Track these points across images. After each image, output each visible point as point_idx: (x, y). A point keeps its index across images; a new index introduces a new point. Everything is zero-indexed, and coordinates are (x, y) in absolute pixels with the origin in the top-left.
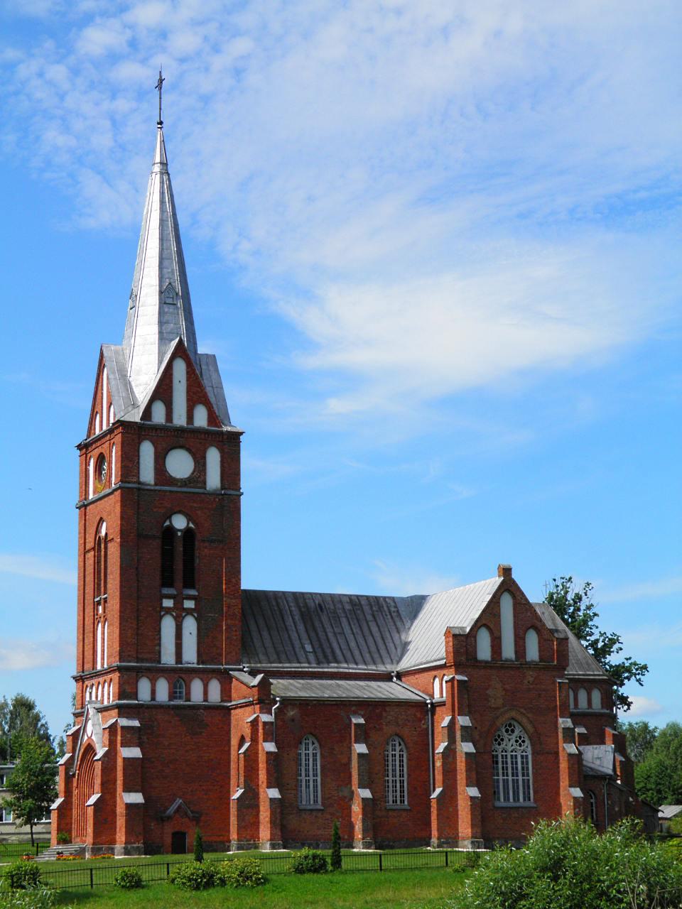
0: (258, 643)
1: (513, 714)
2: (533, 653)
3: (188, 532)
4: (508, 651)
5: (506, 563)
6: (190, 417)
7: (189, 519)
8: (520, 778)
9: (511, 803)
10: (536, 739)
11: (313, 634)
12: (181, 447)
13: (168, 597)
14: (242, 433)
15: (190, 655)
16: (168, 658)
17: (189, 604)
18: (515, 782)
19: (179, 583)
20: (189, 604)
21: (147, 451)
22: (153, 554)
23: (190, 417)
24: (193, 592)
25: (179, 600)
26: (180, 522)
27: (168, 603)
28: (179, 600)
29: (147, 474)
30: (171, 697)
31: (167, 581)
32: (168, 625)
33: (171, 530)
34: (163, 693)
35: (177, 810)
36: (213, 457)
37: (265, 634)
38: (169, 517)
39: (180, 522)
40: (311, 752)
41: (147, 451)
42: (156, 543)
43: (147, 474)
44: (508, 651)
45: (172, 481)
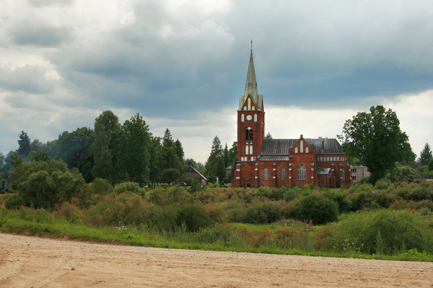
0: (266, 150)
1: (302, 163)
2: (307, 151)
3: (251, 130)
4: (302, 151)
5: (302, 134)
6: (251, 109)
7: (251, 128)
8: (304, 175)
9: (302, 179)
10: (307, 168)
11: (278, 148)
12: (249, 114)
13: (247, 142)
15: (251, 153)
16: (247, 153)
17: (251, 143)
18: (301, 176)
19: (249, 140)
20: (251, 143)
21: (243, 116)
22: (244, 135)
23: (251, 109)
24: (252, 141)
25: (249, 143)
26: (249, 128)
27: (247, 143)
28: (249, 143)
29: (243, 120)
30: (247, 160)
31: (247, 139)
32: (247, 147)
33: (248, 130)
34: (246, 159)
35: (248, 180)
37: (268, 148)
38: (247, 128)
39: (249, 128)
40: (266, 170)
41: (243, 116)
42: (245, 133)
43: (243, 120)
44: (302, 151)
45: (248, 121)
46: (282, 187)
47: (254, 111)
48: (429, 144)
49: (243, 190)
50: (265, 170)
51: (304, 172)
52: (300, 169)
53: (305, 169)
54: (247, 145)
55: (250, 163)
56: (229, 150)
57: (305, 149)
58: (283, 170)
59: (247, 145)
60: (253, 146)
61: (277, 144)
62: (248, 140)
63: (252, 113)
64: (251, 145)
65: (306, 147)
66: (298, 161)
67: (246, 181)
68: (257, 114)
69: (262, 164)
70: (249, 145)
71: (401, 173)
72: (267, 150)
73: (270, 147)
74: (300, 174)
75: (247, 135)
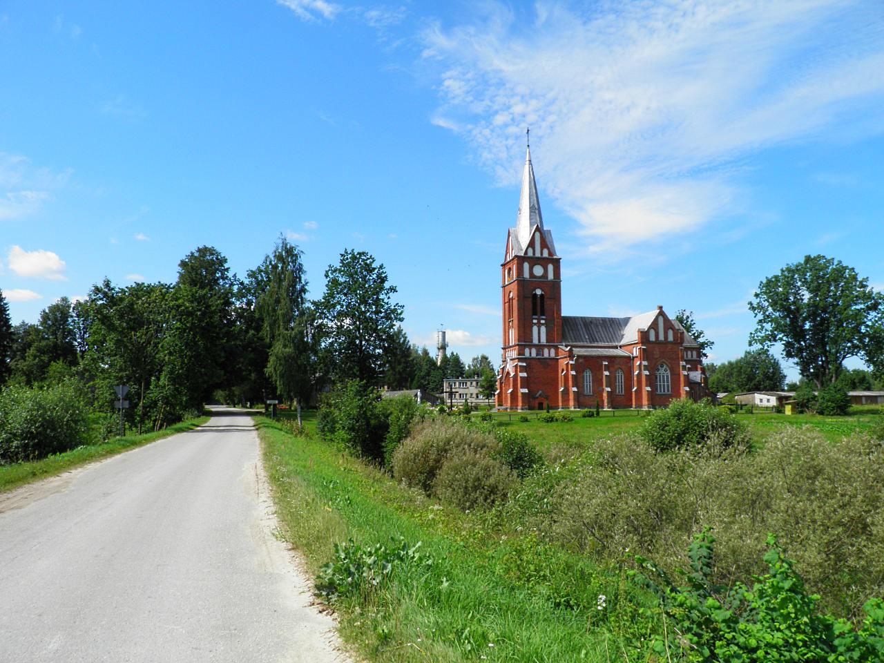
4: (662, 338)
6: (542, 254)
12: (539, 264)
15: (544, 340)
16: (535, 341)
17: (543, 322)
19: (539, 314)
20: (543, 322)
21: (526, 266)
23: (542, 254)
24: (544, 317)
25: (539, 320)
26: (539, 292)
27: (535, 321)
28: (539, 320)
29: (526, 275)
31: (535, 314)
32: (535, 329)
35: (540, 395)
36: (550, 267)
38: (535, 290)
39: (539, 292)
41: (526, 266)
42: (530, 300)
43: (526, 275)
44: (662, 338)
45: (535, 277)
46: (270, 377)
54: (535, 324)
55: (543, 360)
56: (42, 324)
57: (667, 333)
59: (535, 324)
60: (546, 327)
63: (543, 262)
64: (543, 324)
65: (668, 329)
66: (656, 357)
67: (537, 398)
68: (554, 266)
69: (581, 363)
70: (539, 325)
71: (395, 351)
72: (571, 337)
73: (572, 330)
75: (534, 304)
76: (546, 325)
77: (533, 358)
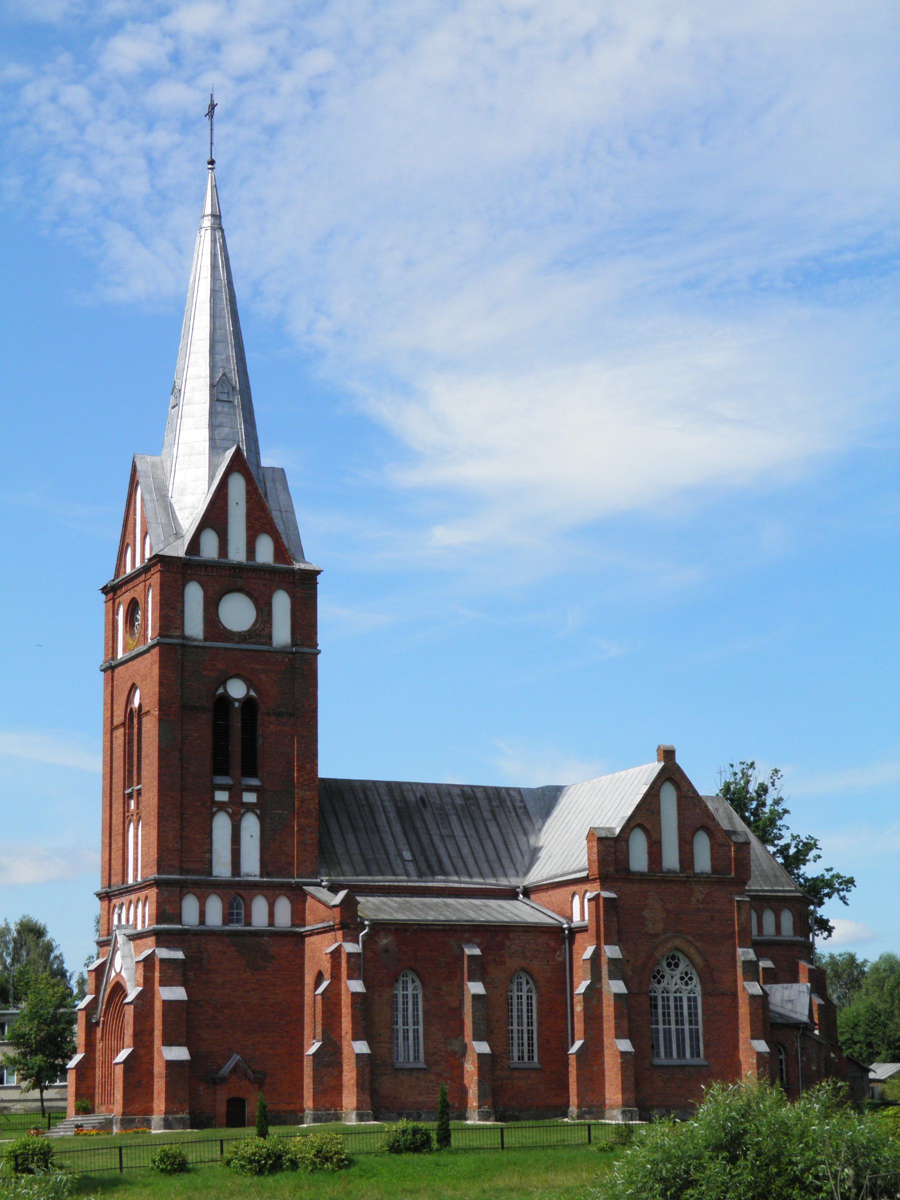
2: (703, 861)
4: (671, 859)
7: (250, 685)
9: (675, 1060)
11: (412, 837)
13: (222, 788)
14: (319, 572)
15: (251, 865)
16: (222, 868)
17: (250, 798)
18: (667, 1032)
20: (250, 798)
21: (194, 595)
24: (254, 782)
25: (236, 792)
26: (237, 690)
27: (222, 796)
28: (236, 792)
31: (221, 767)
32: (222, 825)
33: (225, 700)
36: (281, 603)
38: (224, 683)
39: (237, 690)
41: (194, 595)
42: (206, 718)
44: (671, 859)
47: (263, 570)
48: (826, 868)
49: (260, 1141)
50: (400, 993)
51: (685, 1004)
52: (664, 984)
53: (696, 987)
54: (222, 806)
58: (515, 994)
59: (222, 806)
60: (259, 817)
61: (392, 815)
62: (225, 772)
64: (249, 807)
74: (661, 1018)
75: (221, 734)
76: (262, 811)
77: (213, 933)
